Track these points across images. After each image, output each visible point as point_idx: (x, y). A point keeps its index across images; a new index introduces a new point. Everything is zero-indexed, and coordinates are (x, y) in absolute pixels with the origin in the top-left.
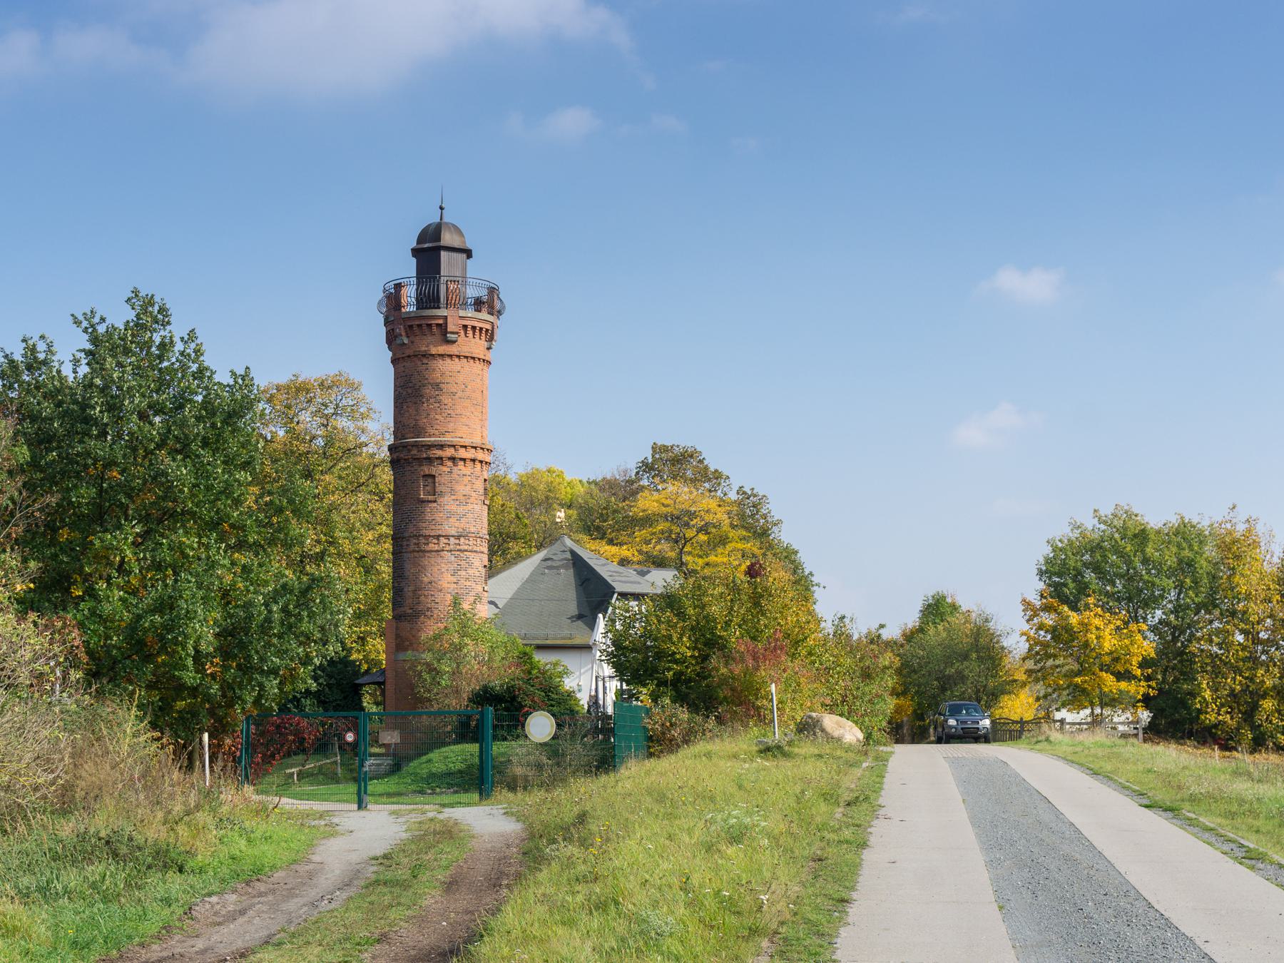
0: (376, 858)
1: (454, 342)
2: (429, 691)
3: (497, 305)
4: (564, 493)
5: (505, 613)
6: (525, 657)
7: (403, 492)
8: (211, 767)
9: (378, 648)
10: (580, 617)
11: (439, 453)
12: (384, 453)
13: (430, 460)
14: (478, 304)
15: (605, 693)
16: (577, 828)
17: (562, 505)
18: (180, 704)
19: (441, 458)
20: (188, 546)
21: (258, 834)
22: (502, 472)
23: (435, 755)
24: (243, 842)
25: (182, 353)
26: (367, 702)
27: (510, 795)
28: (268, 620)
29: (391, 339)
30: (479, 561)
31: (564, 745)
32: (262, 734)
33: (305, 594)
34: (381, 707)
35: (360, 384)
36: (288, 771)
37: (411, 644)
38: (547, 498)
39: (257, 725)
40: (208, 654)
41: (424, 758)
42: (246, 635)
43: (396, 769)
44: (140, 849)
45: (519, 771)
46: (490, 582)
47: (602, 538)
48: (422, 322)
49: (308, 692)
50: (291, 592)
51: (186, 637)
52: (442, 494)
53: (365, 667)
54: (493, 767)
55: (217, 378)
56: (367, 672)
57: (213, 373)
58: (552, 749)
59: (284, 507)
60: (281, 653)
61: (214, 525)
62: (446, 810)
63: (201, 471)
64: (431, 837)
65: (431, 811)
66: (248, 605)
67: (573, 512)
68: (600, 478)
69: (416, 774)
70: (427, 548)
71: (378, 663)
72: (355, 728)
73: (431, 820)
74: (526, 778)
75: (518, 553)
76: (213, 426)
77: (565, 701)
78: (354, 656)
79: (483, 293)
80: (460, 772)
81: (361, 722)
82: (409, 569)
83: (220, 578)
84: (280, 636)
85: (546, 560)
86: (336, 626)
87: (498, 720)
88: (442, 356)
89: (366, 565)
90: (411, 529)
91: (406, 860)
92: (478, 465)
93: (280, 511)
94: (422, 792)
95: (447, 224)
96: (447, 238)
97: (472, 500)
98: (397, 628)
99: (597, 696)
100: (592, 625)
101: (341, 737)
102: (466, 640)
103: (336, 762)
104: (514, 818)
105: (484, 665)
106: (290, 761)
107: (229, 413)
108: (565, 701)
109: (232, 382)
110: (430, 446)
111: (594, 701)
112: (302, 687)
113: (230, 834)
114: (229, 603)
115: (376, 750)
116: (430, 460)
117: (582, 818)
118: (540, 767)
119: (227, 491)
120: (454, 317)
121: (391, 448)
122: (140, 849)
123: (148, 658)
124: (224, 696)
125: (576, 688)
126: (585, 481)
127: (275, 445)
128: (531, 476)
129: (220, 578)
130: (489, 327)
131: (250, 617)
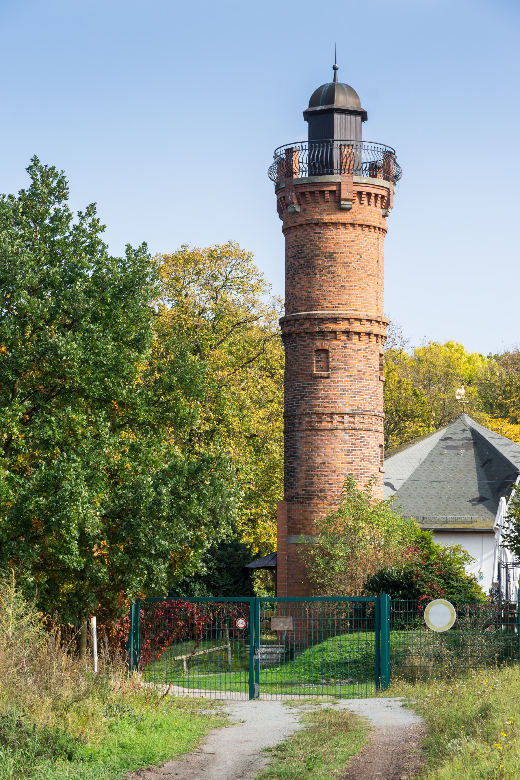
0: (269, 750)
1: (348, 210)
2: (323, 577)
3: (394, 170)
4: (464, 369)
5: (401, 495)
6: (423, 542)
7: (295, 368)
8: (99, 652)
9: (269, 531)
10: (481, 500)
11: (332, 327)
12: (276, 328)
13: (323, 334)
14: (373, 169)
15: (508, 580)
16: (480, 722)
17: (462, 382)
18: (67, 587)
19: (334, 332)
20: (78, 423)
21: (148, 722)
22: (397, 347)
23: (329, 644)
24: (133, 730)
25: (77, 228)
26: (258, 587)
27: (409, 687)
28: (157, 502)
29: (282, 207)
30: (375, 440)
31: (465, 635)
32: (151, 619)
33: (195, 476)
34: (272, 593)
35: (250, 255)
36: (177, 658)
37: (304, 527)
38: (447, 374)
39: (146, 610)
40: (94, 538)
41: (317, 647)
42: (134, 517)
43: (288, 657)
44: (29, 735)
45: (417, 661)
46: (386, 462)
47: (505, 417)
48: (318, 184)
49: (198, 577)
50: (181, 473)
51: (69, 520)
52: (335, 370)
53: (256, 550)
54: (391, 658)
55: (111, 252)
56: (258, 555)
57: (105, 247)
58: (452, 638)
59: (178, 381)
60: (170, 537)
61: (103, 402)
62: (342, 701)
63: (88, 344)
64: (326, 729)
65: (326, 703)
66: (136, 487)
67: (474, 389)
68: (502, 353)
69: (309, 664)
70: (320, 426)
71: (268, 547)
72: (247, 614)
73: (326, 711)
74: (424, 669)
75: (416, 432)
76: (103, 300)
77: (466, 589)
78: (245, 539)
79: (379, 157)
80: (355, 662)
81: (252, 607)
82: (302, 448)
83: (107, 458)
84: (169, 519)
85: (445, 439)
86: (227, 509)
87: (395, 607)
88: (335, 224)
89: (256, 443)
90: (304, 407)
91: (302, 752)
92: (374, 339)
93: (170, 389)
94: (315, 682)
95: (340, 85)
96: (341, 100)
97: (366, 376)
98: (289, 511)
99: (499, 585)
100: (494, 509)
101: (232, 623)
102: (362, 524)
103: (226, 650)
104: (413, 712)
105: (378, 549)
106: (178, 647)
107: (124, 288)
108: (466, 589)
109: (124, 258)
110: (323, 320)
111: (497, 590)
112: (192, 571)
113: (119, 722)
114: (116, 483)
115: (266, 637)
116: (323, 334)
117: (485, 712)
118: (439, 658)
119: (115, 369)
120: (348, 184)
121: (282, 322)
122: (29, 735)
123: (35, 539)
124: (112, 580)
125: (477, 576)
126: (485, 355)
127: (162, 319)
128: (428, 350)
129: (107, 458)
130: (384, 193)
131: (138, 499)
